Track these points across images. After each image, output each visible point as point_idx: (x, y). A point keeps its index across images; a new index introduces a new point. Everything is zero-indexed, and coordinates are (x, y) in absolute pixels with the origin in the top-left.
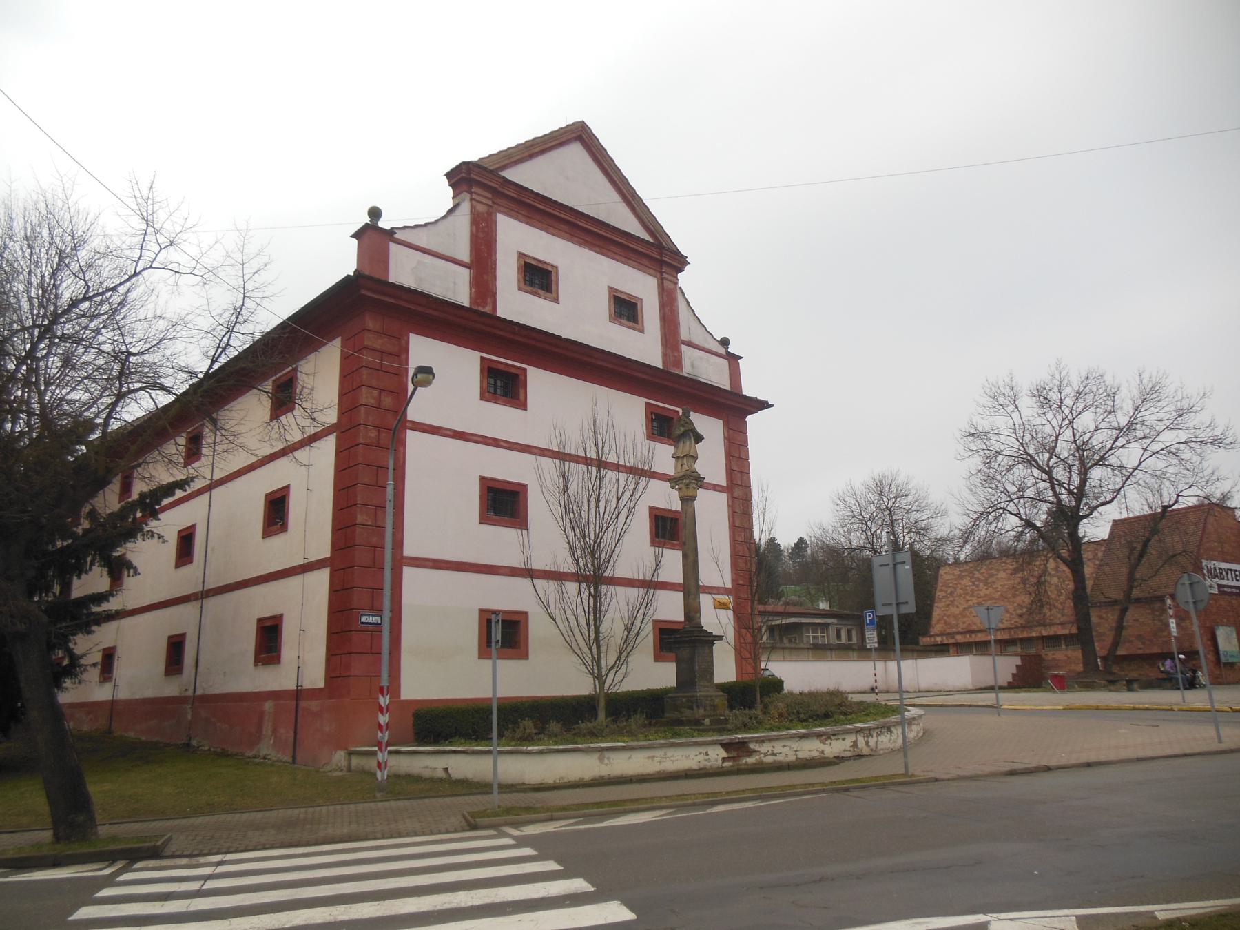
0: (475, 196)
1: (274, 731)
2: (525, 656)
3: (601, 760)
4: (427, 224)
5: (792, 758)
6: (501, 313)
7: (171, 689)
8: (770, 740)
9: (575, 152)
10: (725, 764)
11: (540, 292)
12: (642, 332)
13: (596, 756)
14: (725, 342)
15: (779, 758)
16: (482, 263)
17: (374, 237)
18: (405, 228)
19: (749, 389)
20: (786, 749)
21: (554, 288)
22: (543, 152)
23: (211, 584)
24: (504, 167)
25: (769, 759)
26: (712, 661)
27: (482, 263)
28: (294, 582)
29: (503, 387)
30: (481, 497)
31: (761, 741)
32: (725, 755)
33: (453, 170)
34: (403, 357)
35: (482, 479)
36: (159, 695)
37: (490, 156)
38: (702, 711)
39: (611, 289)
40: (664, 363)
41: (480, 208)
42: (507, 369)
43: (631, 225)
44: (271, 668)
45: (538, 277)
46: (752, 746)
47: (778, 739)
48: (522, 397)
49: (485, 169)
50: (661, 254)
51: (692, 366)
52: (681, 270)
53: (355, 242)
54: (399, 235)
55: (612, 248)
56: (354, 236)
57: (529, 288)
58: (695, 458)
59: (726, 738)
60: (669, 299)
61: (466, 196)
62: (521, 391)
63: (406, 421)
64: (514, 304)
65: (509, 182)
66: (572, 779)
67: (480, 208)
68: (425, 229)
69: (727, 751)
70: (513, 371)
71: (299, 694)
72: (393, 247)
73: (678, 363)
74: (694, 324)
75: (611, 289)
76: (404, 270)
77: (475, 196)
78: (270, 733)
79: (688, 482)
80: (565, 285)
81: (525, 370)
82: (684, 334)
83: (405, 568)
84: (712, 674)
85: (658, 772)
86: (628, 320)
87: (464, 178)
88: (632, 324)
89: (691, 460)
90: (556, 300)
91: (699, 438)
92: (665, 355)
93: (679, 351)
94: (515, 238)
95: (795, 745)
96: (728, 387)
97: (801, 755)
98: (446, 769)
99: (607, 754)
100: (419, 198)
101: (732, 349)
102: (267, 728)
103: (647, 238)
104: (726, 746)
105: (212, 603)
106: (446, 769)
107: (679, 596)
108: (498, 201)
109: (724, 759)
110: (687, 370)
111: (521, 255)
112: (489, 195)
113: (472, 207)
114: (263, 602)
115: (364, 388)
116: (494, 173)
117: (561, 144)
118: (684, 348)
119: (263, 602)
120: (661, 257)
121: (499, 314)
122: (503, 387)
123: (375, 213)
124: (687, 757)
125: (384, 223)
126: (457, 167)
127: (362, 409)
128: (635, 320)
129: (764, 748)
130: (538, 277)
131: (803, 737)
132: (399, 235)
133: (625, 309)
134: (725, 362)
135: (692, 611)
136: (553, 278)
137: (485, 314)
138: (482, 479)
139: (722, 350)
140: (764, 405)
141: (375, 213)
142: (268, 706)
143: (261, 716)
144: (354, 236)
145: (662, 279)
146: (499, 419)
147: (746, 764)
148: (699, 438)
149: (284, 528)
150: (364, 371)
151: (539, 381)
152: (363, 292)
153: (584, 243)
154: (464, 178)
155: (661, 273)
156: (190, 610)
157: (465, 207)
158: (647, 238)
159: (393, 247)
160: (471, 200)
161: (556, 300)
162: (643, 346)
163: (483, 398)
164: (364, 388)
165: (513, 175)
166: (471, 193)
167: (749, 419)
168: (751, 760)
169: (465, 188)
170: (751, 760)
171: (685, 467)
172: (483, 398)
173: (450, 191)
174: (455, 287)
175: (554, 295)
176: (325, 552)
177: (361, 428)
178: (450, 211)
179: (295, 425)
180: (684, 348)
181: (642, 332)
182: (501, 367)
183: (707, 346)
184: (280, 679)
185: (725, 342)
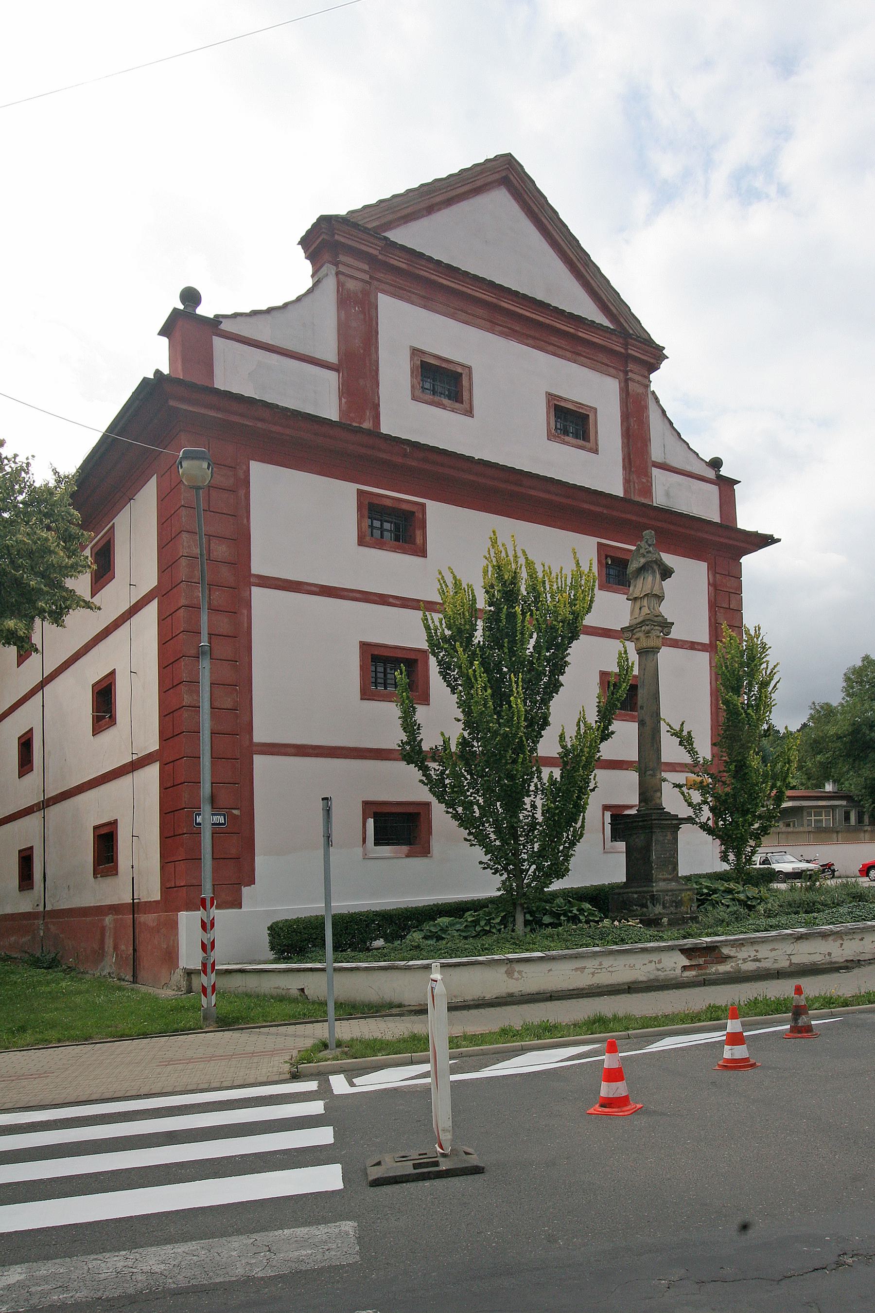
0: (342, 268)
1: (116, 948)
2: (425, 852)
3: (509, 974)
4: (270, 310)
5: (784, 964)
6: (385, 428)
7: (24, 904)
8: (753, 942)
9: (499, 202)
10: (687, 974)
11: (446, 401)
12: (596, 452)
13: (503, 969)
14: (716, 464)
15: (765, 964)
16: (357, 366)
17: (188, 326)
18: (236, 315)
19: (747, 520)
20: (774, 953)
21: (465, 395)
22: (449, 202)
23: (51, 793)
24: (389, 226)
25: (750, 966)
26: (676, 850)
27: (357, 366)
28: (125, 781)
29: (395, 528)
30: (362, 668)
31: (740, 944)
32: (687, 963)
33: (309, 232)
34: (242, 493)
35: (365, 646)
36: (16, 912)
37: (365, 207)
38: (658, 909)
39: (550, 397)
40: (625, 491)
41: (351, 285)
42: (396, 505)
43: (585, 307)
44: (109, 881)
45: (442, 381)
46: (726, 951)
47: (764, 940)
48: (419, 541)
49: (355, 225)
50: (626, 346)
51: (667, 494)
52: (654, 368)
53: (165, 341)
54: (225, 326)
55: (554, 339)
56: (162, 333)
57: (429, 397)
58: (660, 598)
59: (689, 942)
60: (637, 409)
61: (329, 269)
62: (418, 533)
63: (250, 575)
64: (405, 416)
65: (394, 244)
66: (468, 997)
67: (351, 285)
68: (267, 316)
69: (689, 958)
70: (404, 507)
71: (135, 907)
72: (218, 343)
73: (647, 490)
74: (671, 439)
75: (550, 397)
76: (236, 372)
77: (342, 268)
78: (111, 949)
79: (651, 631)
80: (481, 392)
81: (423, 505)
82: (656, 453)
83: (255, 756)
84: (676, 865)
85: (590, 987)
86: (577, 437)
87: (327, 240)
88: (581, 442)
89: (654, 601)
90: (469, 412)
91: (666, 573)
92: (627, 482)
93: (649, 476)
94: (407, 328)
95: (789, 948)
96: (716, 519)
97: (795, 960)
98: (302, 990)
99: (518, 967)
100: (263, 273)
101: (724, 472)
102: (109, 943)
103: (606, 323)
104: (687, 952)
105: (54, 811)
106: (302, 990)
107: (633, 777)
108: (380, 275)
109: (685, 968)
110: (659, 499)
111: (415, 352)
112: (366, 267)
113: (340, 285)
114: (94, 808)
115: (184, 535)
116: (376, 234)
117: (477, 191)
118: (655, 471)
119: (94, 808)
120: (629, 351)
121: (384, 429)
122: (395, 528)
123: (191, 297)
124: (632, 967)
125: (205, 310)
126: (314, 226)
127: (183, 562)
128: (585, 437)
129: (744, 953)
130: (442, 381)
131: (800, 937)
132: (225, 326)
133: (571, 422)
134: (714, 489)
135: (649, 793)
136: (465, 382)
137: (360, 430)
138: (365, 646)
139: (711, 474)
140: (765, 541)
141: (191, 297)
142: (108, 920)
143: (103, 929)
144: (162, 333)
145: (627, 381)
146: (389, 570)
147: (717, 973)
148: (666, 573)
149: (113, 721)
150: (183, 512)
151: (441, 519)
152: (172, 403)
153: (511, 334)
154: (327, 240)
155: (626, 373)
156: (33, 822)
157: (330, 284)
158: (606, 323)
159: (218, 343)
160: (337, 274)
161: (469, 412)
162: (599, 470)
163: (362, 542)
164: (184, 535)
165: (398, 236)
166: (336, 264)
167: (744, 560)
168: (723, 968)
169: (327, 256)
170: (723, 968)
171: (646, 610)
172: (362, 542)
173: (307, 267)
174: (320, 396)
175: (466, 405)
176: (153, 745)
177: (183, 585)
178: (310, 291)
179: (115, 598)
180: (655, 471)
181: (596, 452)
182: (388, 503)
183: (688, 468)
184: (116, 891)
185: (716, 464)
